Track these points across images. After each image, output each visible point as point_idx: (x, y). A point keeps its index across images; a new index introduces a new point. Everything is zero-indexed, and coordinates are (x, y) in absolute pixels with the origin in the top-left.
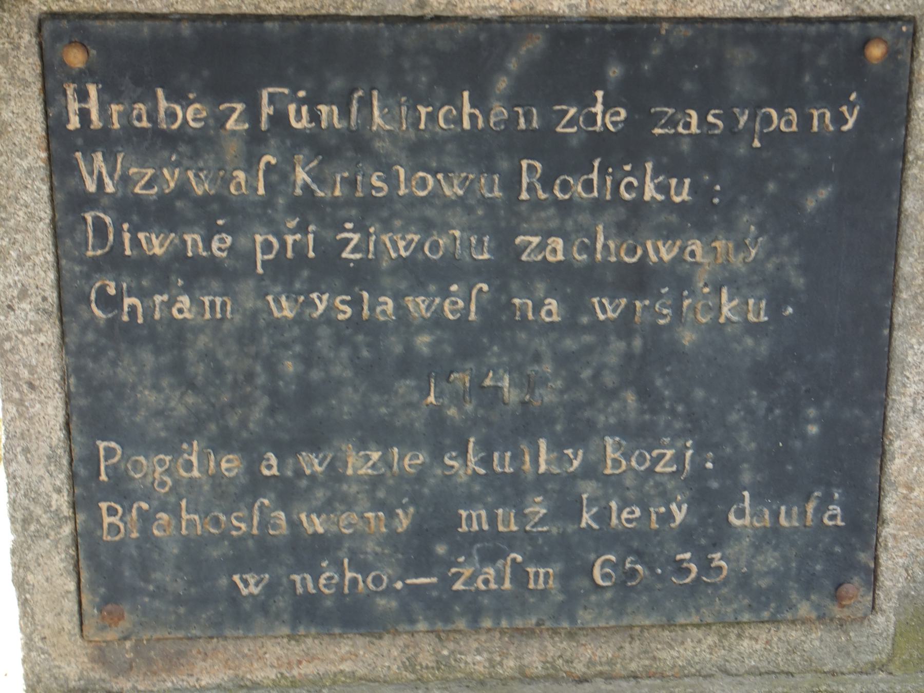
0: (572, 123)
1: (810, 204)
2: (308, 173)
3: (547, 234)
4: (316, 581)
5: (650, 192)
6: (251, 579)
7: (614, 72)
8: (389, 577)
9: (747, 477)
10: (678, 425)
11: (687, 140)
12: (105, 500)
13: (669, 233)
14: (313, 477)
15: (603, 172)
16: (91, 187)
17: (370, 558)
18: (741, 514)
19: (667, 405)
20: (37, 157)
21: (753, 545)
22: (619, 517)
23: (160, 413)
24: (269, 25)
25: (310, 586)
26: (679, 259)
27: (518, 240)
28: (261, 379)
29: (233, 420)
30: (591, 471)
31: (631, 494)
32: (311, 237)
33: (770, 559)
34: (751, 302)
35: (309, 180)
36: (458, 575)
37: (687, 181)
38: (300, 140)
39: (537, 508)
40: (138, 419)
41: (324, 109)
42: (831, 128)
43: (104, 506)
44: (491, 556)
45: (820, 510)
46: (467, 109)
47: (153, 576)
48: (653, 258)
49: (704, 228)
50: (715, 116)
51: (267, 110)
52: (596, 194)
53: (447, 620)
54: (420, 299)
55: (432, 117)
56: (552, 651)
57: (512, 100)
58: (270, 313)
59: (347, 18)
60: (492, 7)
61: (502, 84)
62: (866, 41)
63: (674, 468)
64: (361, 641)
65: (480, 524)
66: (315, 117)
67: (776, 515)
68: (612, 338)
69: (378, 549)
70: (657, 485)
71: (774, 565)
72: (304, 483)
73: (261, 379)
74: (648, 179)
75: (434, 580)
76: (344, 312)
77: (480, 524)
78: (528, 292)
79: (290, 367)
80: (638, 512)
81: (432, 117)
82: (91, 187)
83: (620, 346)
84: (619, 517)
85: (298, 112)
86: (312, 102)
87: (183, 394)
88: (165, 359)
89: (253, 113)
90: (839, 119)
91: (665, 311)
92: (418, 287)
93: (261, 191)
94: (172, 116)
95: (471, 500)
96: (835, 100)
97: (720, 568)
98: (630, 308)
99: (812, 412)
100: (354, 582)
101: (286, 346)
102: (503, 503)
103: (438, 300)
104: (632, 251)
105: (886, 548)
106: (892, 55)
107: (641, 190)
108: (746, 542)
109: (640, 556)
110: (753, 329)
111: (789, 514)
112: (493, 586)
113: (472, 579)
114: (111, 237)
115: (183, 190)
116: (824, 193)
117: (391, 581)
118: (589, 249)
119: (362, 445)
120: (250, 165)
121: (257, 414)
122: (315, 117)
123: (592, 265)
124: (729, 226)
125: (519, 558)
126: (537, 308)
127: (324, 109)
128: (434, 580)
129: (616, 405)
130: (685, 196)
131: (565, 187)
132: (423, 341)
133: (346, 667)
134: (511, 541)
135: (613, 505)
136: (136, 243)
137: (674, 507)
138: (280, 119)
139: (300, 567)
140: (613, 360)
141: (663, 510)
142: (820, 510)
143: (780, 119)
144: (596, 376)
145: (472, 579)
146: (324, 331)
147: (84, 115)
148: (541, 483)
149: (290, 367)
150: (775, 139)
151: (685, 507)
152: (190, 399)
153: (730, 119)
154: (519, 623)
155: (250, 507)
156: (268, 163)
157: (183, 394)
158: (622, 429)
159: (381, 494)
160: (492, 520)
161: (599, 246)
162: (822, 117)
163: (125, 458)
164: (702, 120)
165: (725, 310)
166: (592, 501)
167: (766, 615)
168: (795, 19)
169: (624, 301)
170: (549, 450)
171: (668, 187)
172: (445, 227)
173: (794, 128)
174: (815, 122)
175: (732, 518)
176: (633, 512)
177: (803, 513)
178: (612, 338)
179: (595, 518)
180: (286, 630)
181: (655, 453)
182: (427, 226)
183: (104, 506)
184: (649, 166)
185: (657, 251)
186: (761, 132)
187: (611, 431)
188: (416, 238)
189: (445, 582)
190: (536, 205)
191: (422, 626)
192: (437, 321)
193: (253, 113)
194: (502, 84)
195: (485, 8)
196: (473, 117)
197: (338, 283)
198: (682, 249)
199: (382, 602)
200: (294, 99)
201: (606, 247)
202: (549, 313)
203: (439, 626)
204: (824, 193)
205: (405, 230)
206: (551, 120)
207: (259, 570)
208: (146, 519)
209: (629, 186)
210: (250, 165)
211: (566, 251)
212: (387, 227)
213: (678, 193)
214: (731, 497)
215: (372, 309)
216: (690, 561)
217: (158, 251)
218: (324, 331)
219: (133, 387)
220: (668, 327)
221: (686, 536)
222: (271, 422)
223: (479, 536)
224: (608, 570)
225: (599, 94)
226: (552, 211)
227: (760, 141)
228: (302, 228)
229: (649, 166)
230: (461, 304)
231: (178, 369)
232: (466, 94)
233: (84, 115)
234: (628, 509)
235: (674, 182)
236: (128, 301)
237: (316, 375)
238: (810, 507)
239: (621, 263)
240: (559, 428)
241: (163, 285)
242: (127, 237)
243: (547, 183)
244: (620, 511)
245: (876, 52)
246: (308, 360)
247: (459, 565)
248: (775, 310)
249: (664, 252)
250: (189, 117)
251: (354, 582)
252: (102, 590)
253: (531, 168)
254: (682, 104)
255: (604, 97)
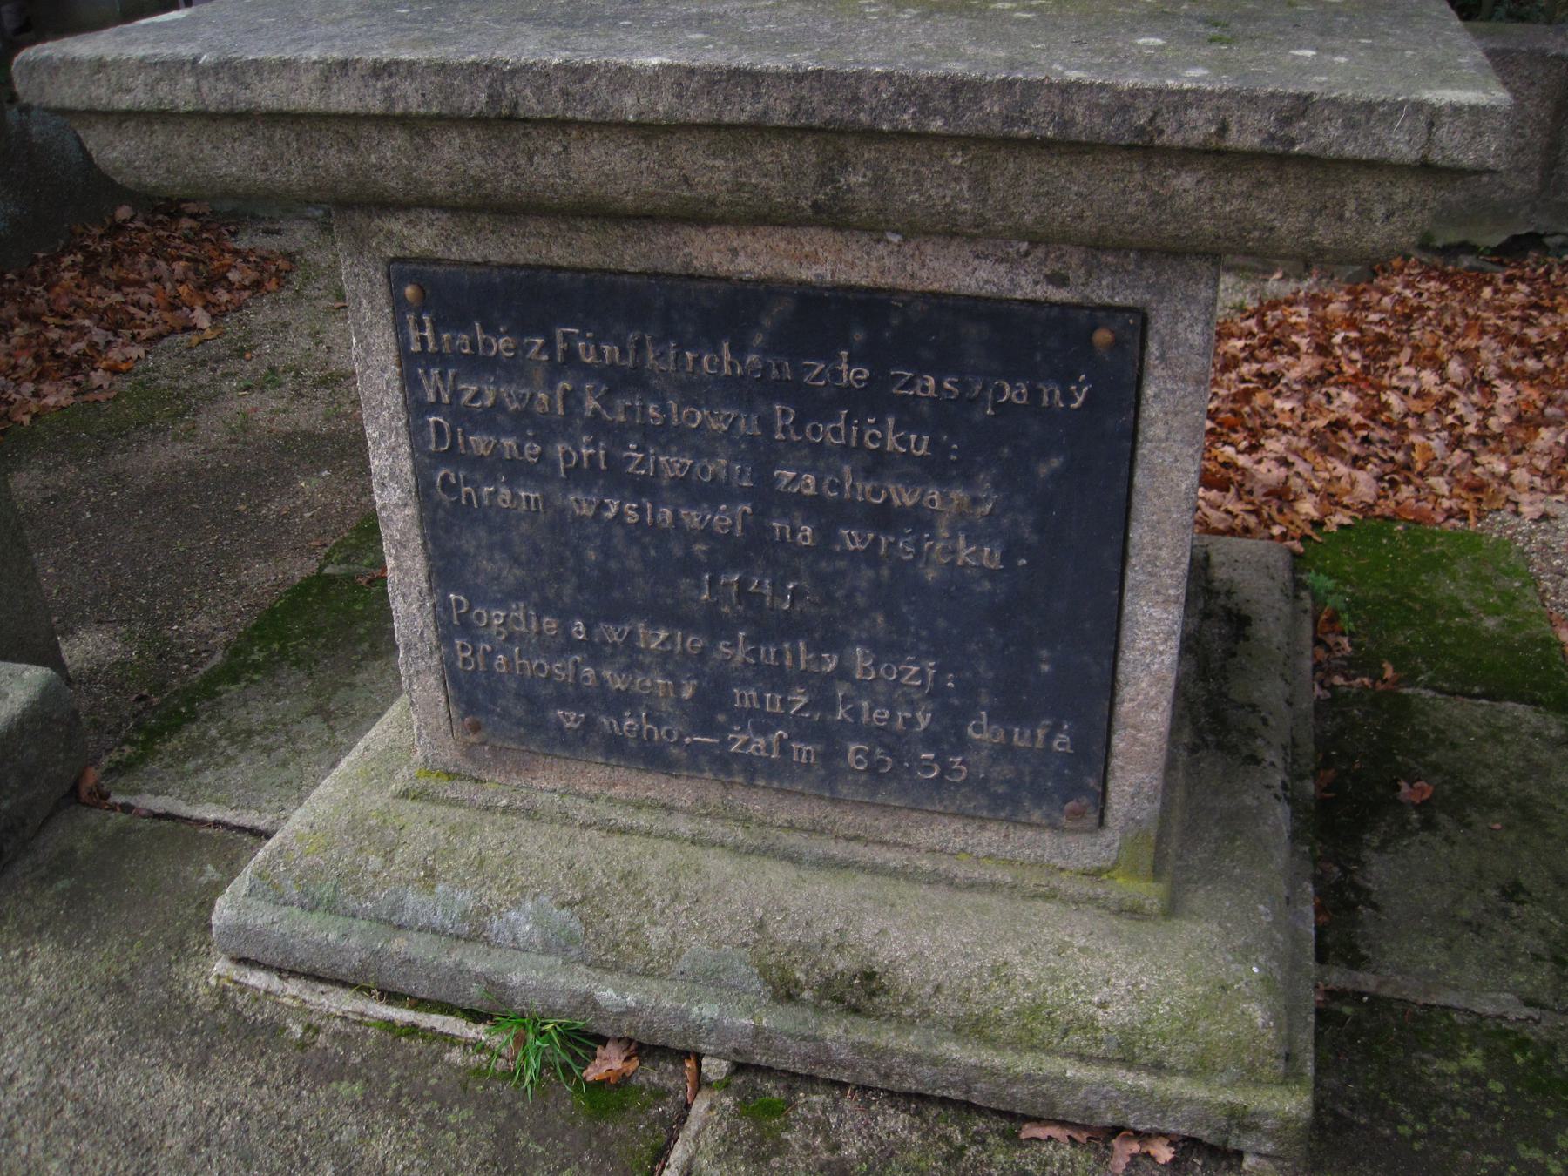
0: (819, 377)
1: (1043, 471)
2: (597, 400)
3: (801, 471)
4: (620, 725)
5: (891, 442)
6: (573, 715)
7: (858, 336)
8: (680, 732)
9: (985, 699)
10: (923, 647)
11: (927, 402)
12: (460, 638)
13: (911, 481)
14: (614, 644)
15: (848, 423)
16: (431, 398)
17: (664, 716)
18: (978, 729)
19: (912, 629)
20: (393, 372)
21: (990, 756)
22: (871, 716)
23: (496, 578)
24: (561, 275)
25: (616, 728)
26: (917, 506)
27: (776, 473)
28: (571, 563)
29: (551, 593)
30: (843, 673)
31: (882, 698)
32: (602, 452)
33: (1005, 770)
34: (987, 549)
35: (598, 406)
36: (734, 740)
37: (926, 438)
38: (588, 372)
39: (800, 699)
40: (479, 581)
41: (607, 348)
42: (1062, 405)
43: (458, 642)
44: (764, 731)
45: (1049, 737)
46: (727, 357)
47: (500, 701)
48: (897, 502)
49: (944, 481)
50: (950, 383)
51: (561, 346)
52: (844, 441)
53: (729, 773)
54: (694, 513)
55: (697, 361)
56: (817, 813)
57: (764, 351)
58: (574, 512)
59: (626, 272)
60: (747, 272)
61: (758, 340)
62: (1095, 328)
63: (918, 683)
64: (663, 778)
65: (751, 703)
66: (600, 354)
67: (1009, 735)
68: (863, 566)
69: (671, 710)
70: (904, 694)
71: (1010, 776)
72: (608, 650)
73: (571, 563)
74: (890, 433)
75: (716, 741)
76: (631, 508)
77: (751, 703)
78: (785, 515)
79: (592, 555)
80: (887, 713)
81: (697, 361)
82: (431, 398)
83: (868, 573)
84: (871, 716)
85: (587, 349)
86: (597, 342)
87: (511, 567)
88: (497, 538)
89: (549, 346)
90: (1068, 397)
91: (909, 549)
92: (693, 503)
93: (561, 411)
94: (488, 345)
95: (745, 683)
96: (1066, 378)
97: (959, 771)
98: (876, 541)
99: (1044, 653)
100: (650, 732)
101: (587, 538)
102: (773, 690)
103: (709, 517)
104: (876, 493)
105: (1114, 778)
106: (1117, 344)
107: (884, 440)
108: (984, 753)
109: (890, 750)
110: (991, 575)
111: (1021, 735)
112: (763, 753)
113: (747, 744)
114: (449, 440)
115: (498, 405)
116: (1056, 462)
117: (681, 736)
118: (839, 487)
119: (653, 624)
120: (551, 385)
121: (568, 591)
122: (600, 354)
123: (840, 503)
124: (968, 480)
125: (785, 736)
126: (794, 533)
127: (607, 348)
128: (716, 741)
129: (866, 623)
130: (923, 451)
131: (815, 430)
132: (699, 548)
133: (651, 794)
134: (778, 720)
135: (865, 704)
136: (466, 442)
137: (919, 714)
138: (571, 354)
139: (608, 712)
140: (864, 585)
141: (908, 715)
142: (1049, 737)
143: (1011, 391)
144: (849, 596)
145: (747, 744)
146: (618, 531)
147: (423, 340)
148: (803, 678)
149: (592, 555)
150: (1004, 409)
151: (929, 715)
152: (518, 572)
153: (963, 386)
154: (787, 785)
155: (567, 660)
156: (565, 390)
157: (511, 567)
158: (872, 644)
159: (670, 667)
160: (762, 700)
161: (847, 486)
162: (1051, 394)
163: (471, 609)
164: (939, 384)
165: (963, 554)
166: (846, 699)
167: (1003, 815)
168: (1024, 301)
169: (871, 536)
170: (808, 651)
171: (909, 441)
172: (713, 456)
173: (1024, 401)
174: (1045, 398)
175: (970, 730)
176: (883, 714)
177: (1034, 737)
178: (863, 566)
179: (849, 712)
180: (600, 759)
181: (902, 667)
182: (698, 454)
183: (458, 642)
184: (891, 422)
185: (900, 496)
186: (995, 400)
187: (860, 642)
188: (689, 462)
189: (726, 744)
190: (793, 445)
191: (707, 775)
192: (707, 533)
193: (549, 346)
194: (758, 340)
195: (742, 272)
196: (731, 364)
197: (627, 494)
198: (922, 495)
199: (674, 751)
200: (582, 337)
201: (853, 486)
202: (805, 538)
203: (722, 777)
204: (1056, 462)
205: (680, 453)
206: (799, 371)
207: (578, 709)
208: (490, 656)
209: (873, 438)
210: (551, 385)
211: (818, 486)
212: (665, 449)
213: (917, 448)
214: (967, 713)
215: (654, 515)
216: (933, 761)
217: (482, 450)
218: (618, 531)
219: (475, 556)
220: (913, 562)
221: (931, 739)
222: (580, 598)
223: (751, 712)
224: (860, 756)
225: (844, 353)
226: (805, 452)
227: (993, 409)
228: (594, 444)
229: (891, 422)
230: (729, 521)
231: (505, 546)
232: (726, 345)
233: (423, 340)
234: (878, 711)
235: (913, 437)
236: (464, 489)
237: (613, 565)
238: (1041, 733)
239: (866, 503)
240: (817, 635)
241: (491, 479)
242: (460, 439)
243: (799, 425)
244: (871, 710)
245: (1102, 336)
246: (606, 552)
247: (732, 731)
248: (1007, 557)
249: (905, 498)
250: (501, 347)
251: (650, 732)
252: (463, 706)
253: (785, 414)
254: (921, 368)
255: (849, 356)
